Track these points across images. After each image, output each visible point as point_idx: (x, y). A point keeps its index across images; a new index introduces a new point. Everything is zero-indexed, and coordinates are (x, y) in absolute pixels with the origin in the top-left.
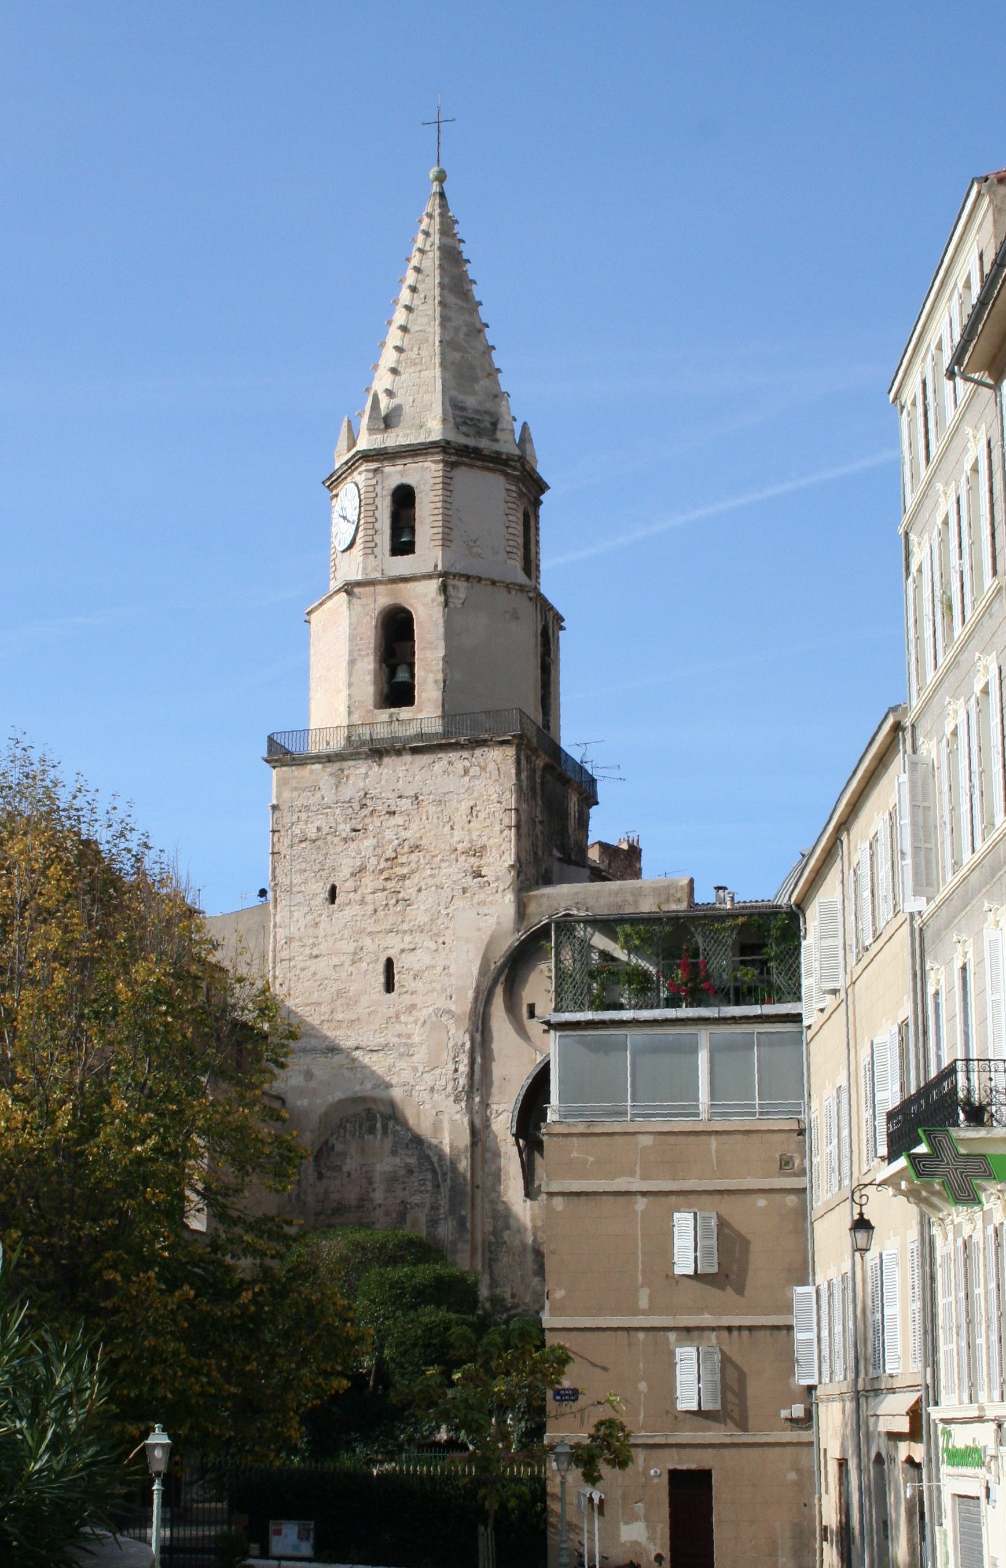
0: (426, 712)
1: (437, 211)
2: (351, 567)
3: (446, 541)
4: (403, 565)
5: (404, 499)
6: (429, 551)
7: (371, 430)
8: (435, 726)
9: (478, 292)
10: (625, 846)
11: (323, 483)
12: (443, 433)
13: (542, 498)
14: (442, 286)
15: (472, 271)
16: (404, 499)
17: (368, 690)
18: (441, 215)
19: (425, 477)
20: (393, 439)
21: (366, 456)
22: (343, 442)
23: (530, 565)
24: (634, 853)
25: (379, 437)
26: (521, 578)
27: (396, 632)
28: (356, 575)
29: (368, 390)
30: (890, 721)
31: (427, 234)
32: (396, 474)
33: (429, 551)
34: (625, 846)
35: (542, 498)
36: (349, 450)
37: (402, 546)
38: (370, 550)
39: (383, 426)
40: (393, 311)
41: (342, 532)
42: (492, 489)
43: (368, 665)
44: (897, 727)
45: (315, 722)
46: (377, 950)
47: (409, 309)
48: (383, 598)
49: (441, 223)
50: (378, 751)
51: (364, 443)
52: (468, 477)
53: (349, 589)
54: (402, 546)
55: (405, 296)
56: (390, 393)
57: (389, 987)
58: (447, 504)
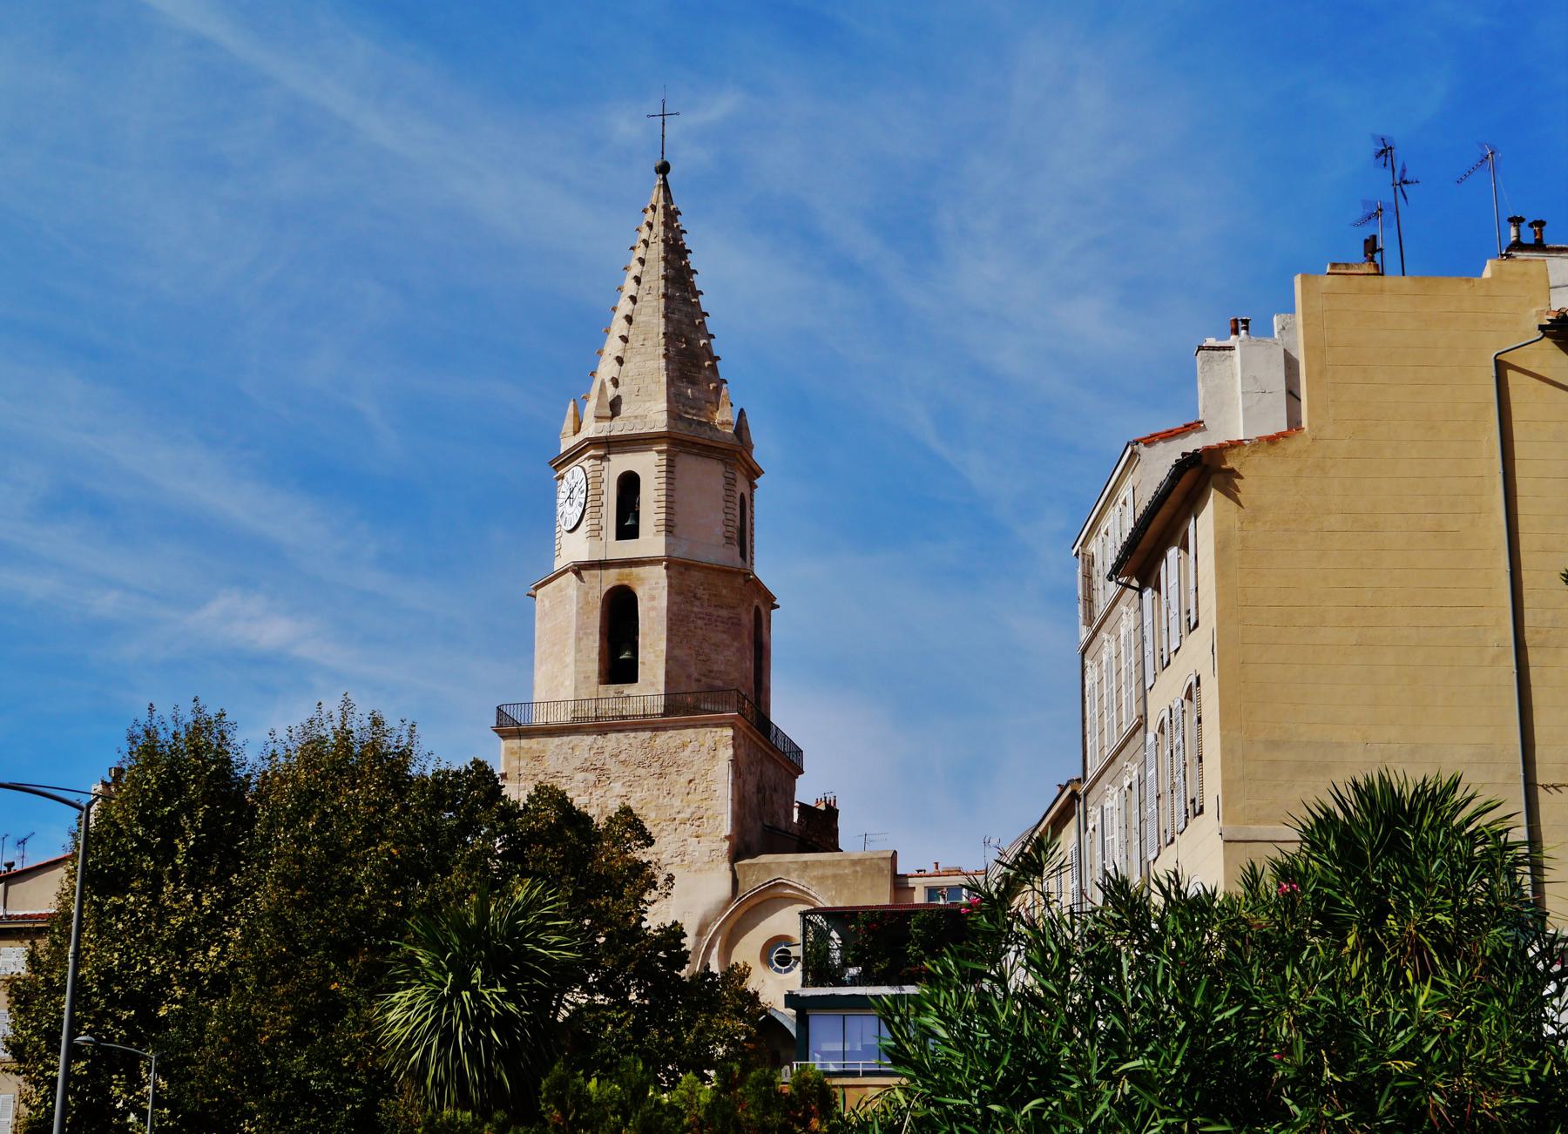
0: (650, 687)
1: (662, 203)
2: (574, 548)
3: (670, 528)
4: (628, 549)
5: (629, 485)
6: (651, 541)
7: (599, 418)
8: (657, 705)
9: (698, 282)
10: (822, 807)
11: (551, 463)
12: (668, 425)
13: (756, 482)
14: (665, 278)
15: (693, 261)
16: (629, 485)
17: (593, 667)
18: (666, 207)
19: (648, 466)
20: (618, 428)
21: (594, 443)
22: (568, 424)
23: (742, 538)
24: (831, 813)
25: (607, 424)
26: (738, 562)
27: (619, 614)
28: (584, 556)
29: (593, 374)
30: (1069, 791)
31: (650, 226)
32: (621, 463)
33: (651, 541)
34: (822, 807)
35: (756, 482)
36: (575, 433)
37: (627, 529)
38: (596, 533)
39: (609, 413)
40: (618, 299)
41: (568, 512)
42: (708, 476)
43: (594, 643)
44: (1074, 795)
45: (539, 695)
47: (633, 299)
48: (611, 578)
49: (665, 215)
50: (602, 727)
51: (591, 429)
52: (691, 466)
53: (579, 569)
54: (627, 529)
55: (630, 287)
56: (615, 382)
58: (670, 495)
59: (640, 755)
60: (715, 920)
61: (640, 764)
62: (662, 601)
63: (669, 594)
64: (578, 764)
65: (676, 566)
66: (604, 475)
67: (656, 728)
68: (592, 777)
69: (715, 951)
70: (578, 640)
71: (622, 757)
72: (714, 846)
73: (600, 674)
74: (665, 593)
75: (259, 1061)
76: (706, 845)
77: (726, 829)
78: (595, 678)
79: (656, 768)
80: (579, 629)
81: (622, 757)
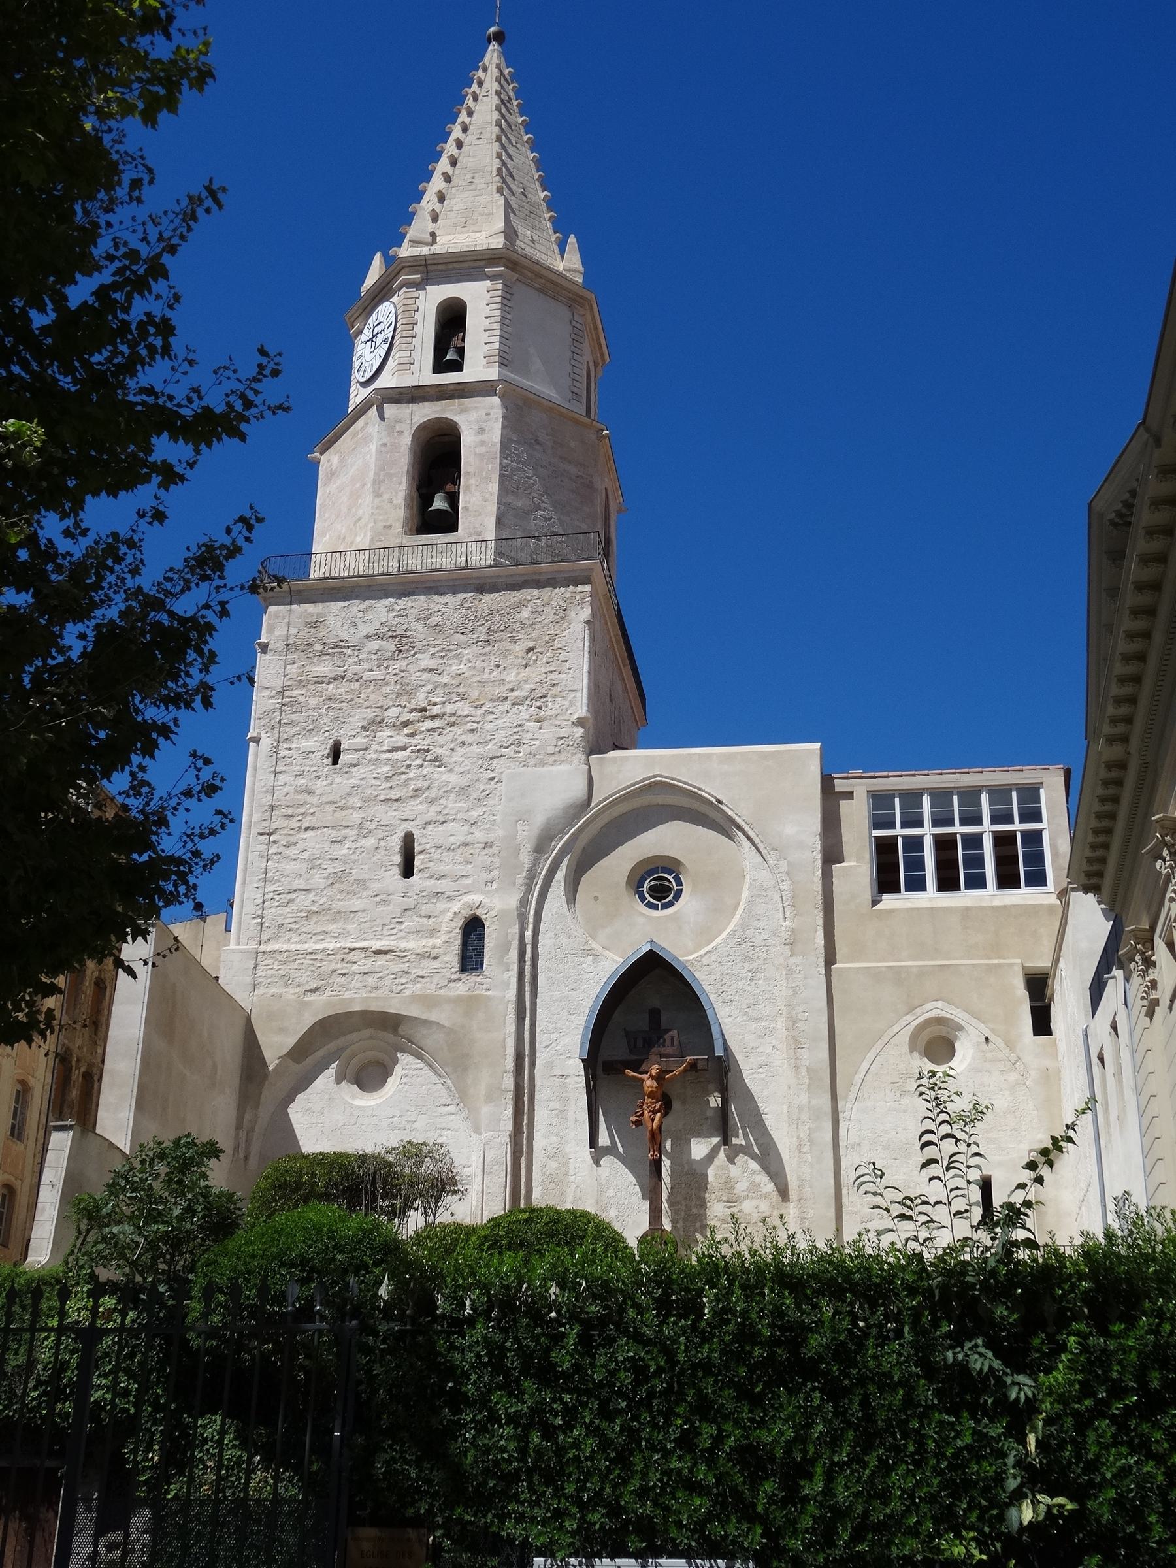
8: (484, 556)
16: (452, 321)
19: (480, 299)
46: (394, 823)
48: (426, 412)
57: (408, 870)
59: (457, 617)
60: (563, 832)
61: (460, 630)
62: (1065, 846)
63: (504, 427)
64: (370, 630)
65: (520, 410)
66: (420, 303)
67: (482, 588)
68: (390, 646)
69: (560, 875)
70: (377, 483)
71: (434, 620)
72: (563, 732)
73: (406, 523)
74: (499, 425)
75: (171, 1289)
76: (549, 732)
77: (580, 707)
78: (398, 527)
79: (481, 633)
80: (380, 469)
81: (434, 620)
